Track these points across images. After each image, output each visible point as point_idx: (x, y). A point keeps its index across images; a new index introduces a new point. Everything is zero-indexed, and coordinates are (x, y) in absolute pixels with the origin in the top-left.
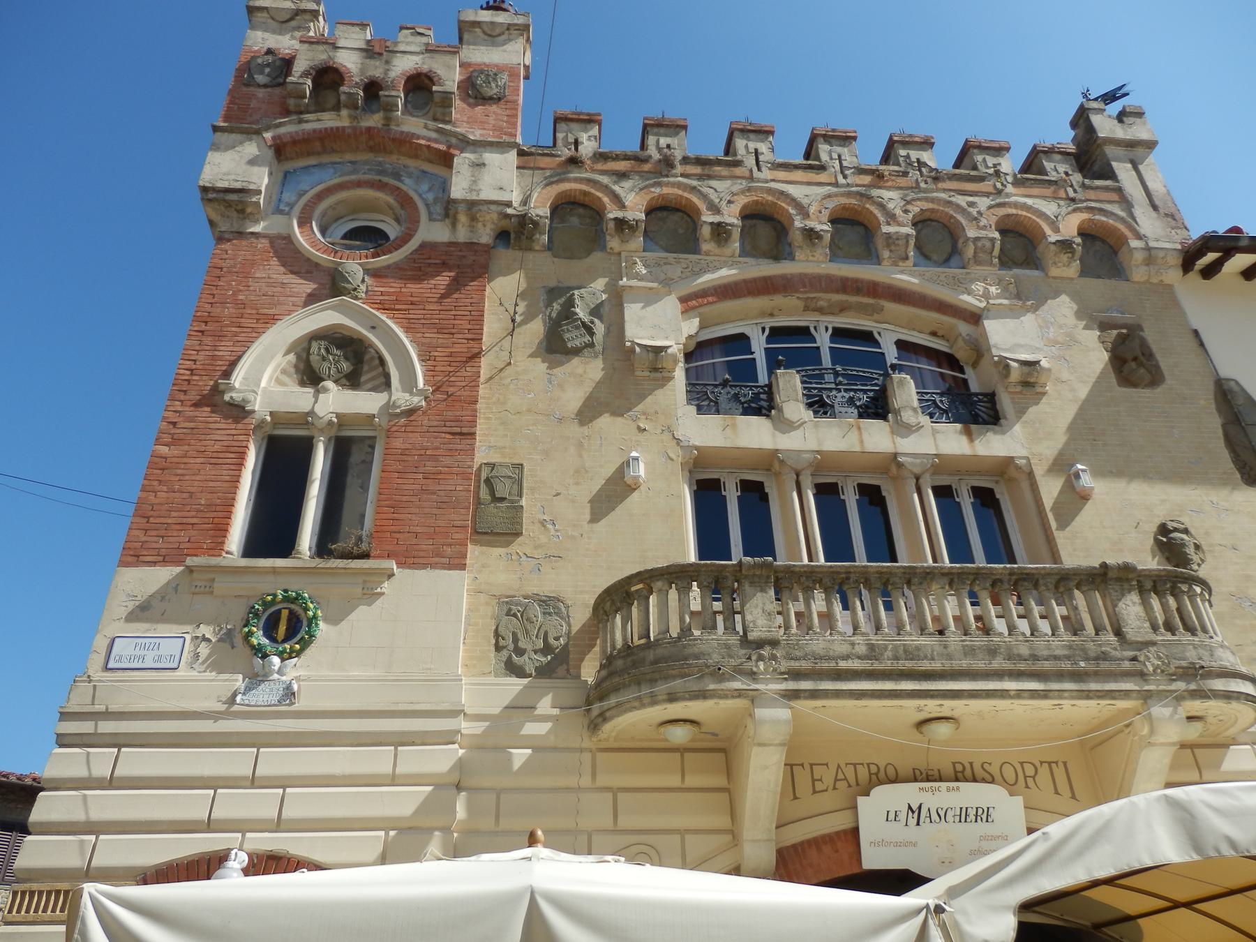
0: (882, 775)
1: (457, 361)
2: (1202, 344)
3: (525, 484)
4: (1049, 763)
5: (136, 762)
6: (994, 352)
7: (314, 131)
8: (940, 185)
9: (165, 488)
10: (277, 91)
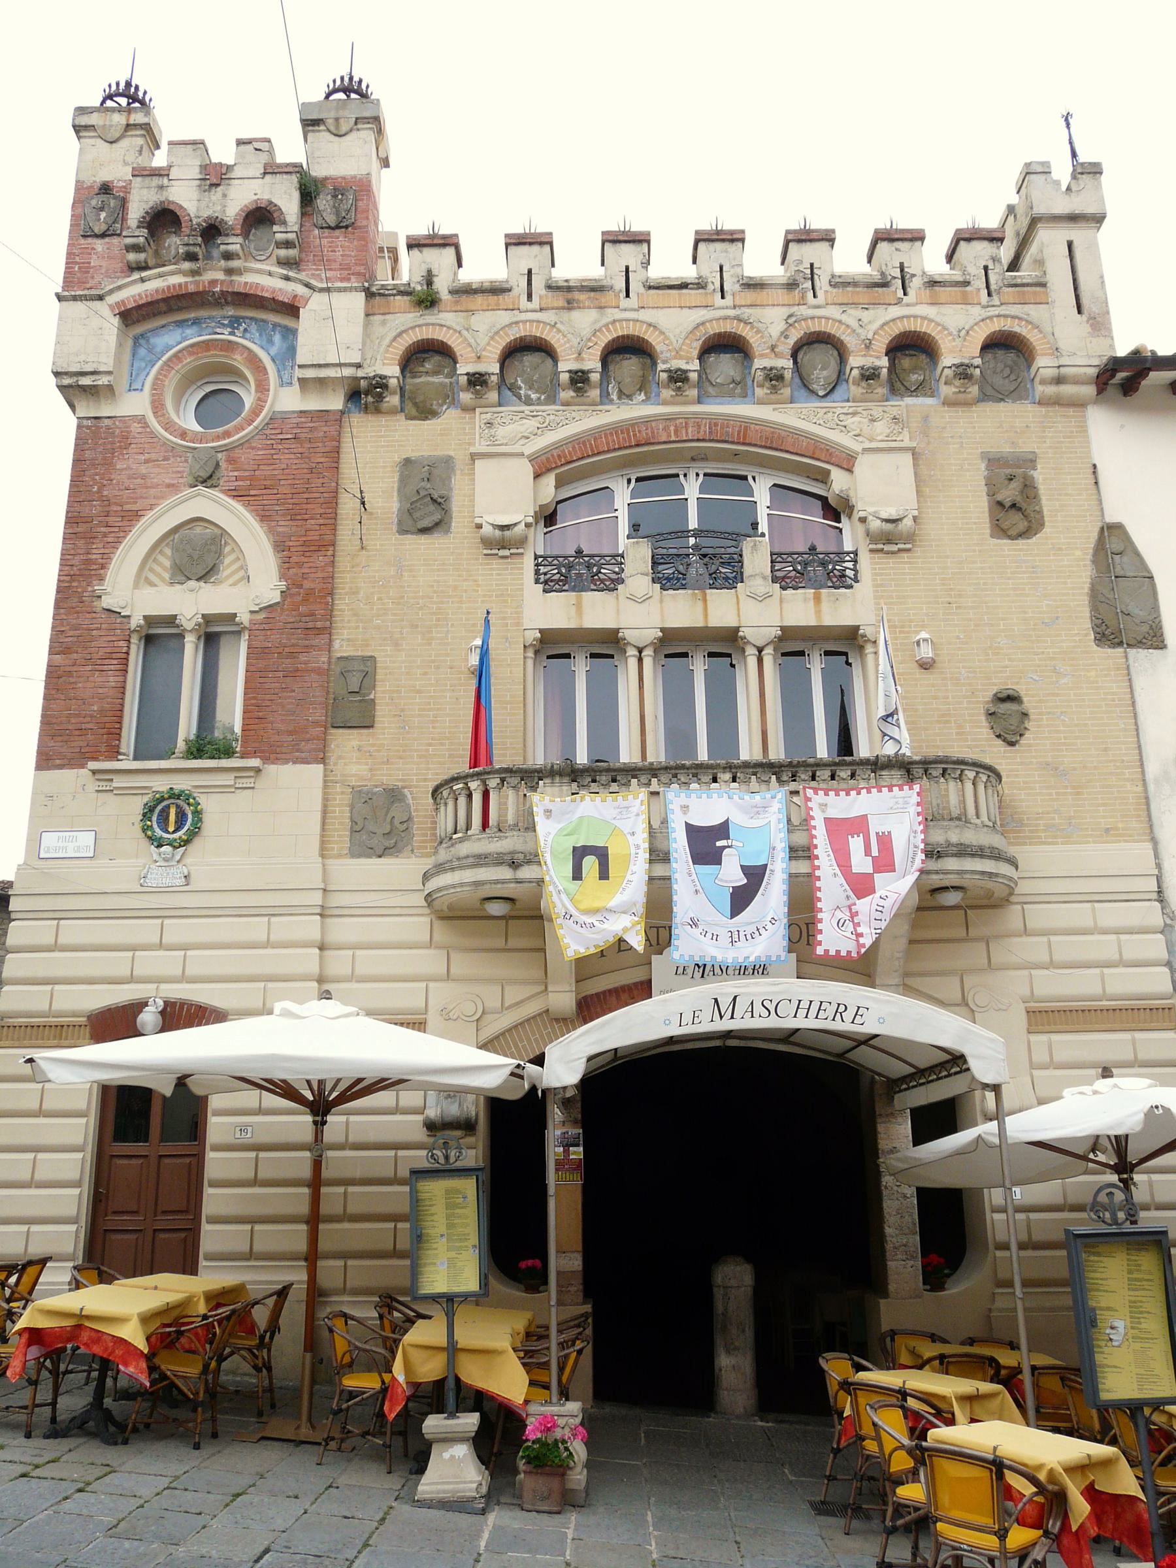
5: (73, 932)
7: (157, 291)
9: (63, 697)
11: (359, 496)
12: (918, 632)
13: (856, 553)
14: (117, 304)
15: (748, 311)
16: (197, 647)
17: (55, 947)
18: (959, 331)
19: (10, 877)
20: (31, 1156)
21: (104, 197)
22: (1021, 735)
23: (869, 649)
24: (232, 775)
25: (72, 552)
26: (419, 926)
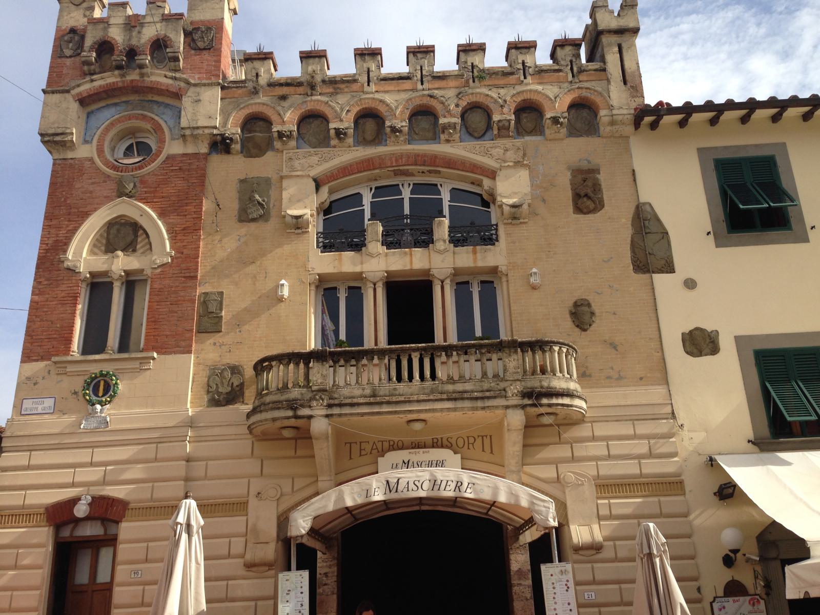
0: (395, 446)
1: (186, 233)
2: (635, 180)
3: (224, 303)
4: (483, 437)
5: (39, 458)
6: (499, 199)
7: (100, 86)
8: (487, 82)
9: (39, 319)
10: (77, 59)
11: (215, 201)
12: (532, 269)
13: (497, 225)
14: (78, 94)
15: (436, 92)
16: (86, 290)
17: (29, 467)
18: (556, 98)
19: (4, 426)
20: (9, 593)
21: (71, 35)
22: (590, 325)
23: (504, 279)
24: (138, 362)
25: (48, 236)
26: (245, 445)
